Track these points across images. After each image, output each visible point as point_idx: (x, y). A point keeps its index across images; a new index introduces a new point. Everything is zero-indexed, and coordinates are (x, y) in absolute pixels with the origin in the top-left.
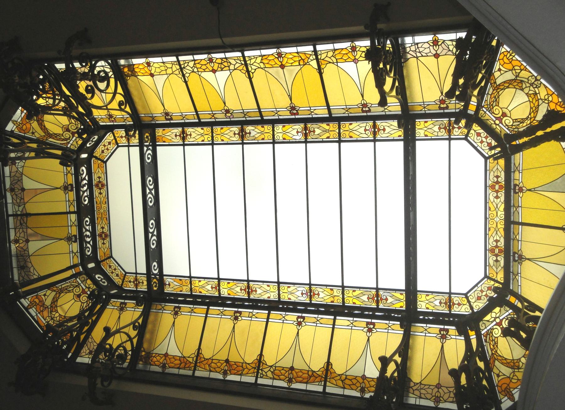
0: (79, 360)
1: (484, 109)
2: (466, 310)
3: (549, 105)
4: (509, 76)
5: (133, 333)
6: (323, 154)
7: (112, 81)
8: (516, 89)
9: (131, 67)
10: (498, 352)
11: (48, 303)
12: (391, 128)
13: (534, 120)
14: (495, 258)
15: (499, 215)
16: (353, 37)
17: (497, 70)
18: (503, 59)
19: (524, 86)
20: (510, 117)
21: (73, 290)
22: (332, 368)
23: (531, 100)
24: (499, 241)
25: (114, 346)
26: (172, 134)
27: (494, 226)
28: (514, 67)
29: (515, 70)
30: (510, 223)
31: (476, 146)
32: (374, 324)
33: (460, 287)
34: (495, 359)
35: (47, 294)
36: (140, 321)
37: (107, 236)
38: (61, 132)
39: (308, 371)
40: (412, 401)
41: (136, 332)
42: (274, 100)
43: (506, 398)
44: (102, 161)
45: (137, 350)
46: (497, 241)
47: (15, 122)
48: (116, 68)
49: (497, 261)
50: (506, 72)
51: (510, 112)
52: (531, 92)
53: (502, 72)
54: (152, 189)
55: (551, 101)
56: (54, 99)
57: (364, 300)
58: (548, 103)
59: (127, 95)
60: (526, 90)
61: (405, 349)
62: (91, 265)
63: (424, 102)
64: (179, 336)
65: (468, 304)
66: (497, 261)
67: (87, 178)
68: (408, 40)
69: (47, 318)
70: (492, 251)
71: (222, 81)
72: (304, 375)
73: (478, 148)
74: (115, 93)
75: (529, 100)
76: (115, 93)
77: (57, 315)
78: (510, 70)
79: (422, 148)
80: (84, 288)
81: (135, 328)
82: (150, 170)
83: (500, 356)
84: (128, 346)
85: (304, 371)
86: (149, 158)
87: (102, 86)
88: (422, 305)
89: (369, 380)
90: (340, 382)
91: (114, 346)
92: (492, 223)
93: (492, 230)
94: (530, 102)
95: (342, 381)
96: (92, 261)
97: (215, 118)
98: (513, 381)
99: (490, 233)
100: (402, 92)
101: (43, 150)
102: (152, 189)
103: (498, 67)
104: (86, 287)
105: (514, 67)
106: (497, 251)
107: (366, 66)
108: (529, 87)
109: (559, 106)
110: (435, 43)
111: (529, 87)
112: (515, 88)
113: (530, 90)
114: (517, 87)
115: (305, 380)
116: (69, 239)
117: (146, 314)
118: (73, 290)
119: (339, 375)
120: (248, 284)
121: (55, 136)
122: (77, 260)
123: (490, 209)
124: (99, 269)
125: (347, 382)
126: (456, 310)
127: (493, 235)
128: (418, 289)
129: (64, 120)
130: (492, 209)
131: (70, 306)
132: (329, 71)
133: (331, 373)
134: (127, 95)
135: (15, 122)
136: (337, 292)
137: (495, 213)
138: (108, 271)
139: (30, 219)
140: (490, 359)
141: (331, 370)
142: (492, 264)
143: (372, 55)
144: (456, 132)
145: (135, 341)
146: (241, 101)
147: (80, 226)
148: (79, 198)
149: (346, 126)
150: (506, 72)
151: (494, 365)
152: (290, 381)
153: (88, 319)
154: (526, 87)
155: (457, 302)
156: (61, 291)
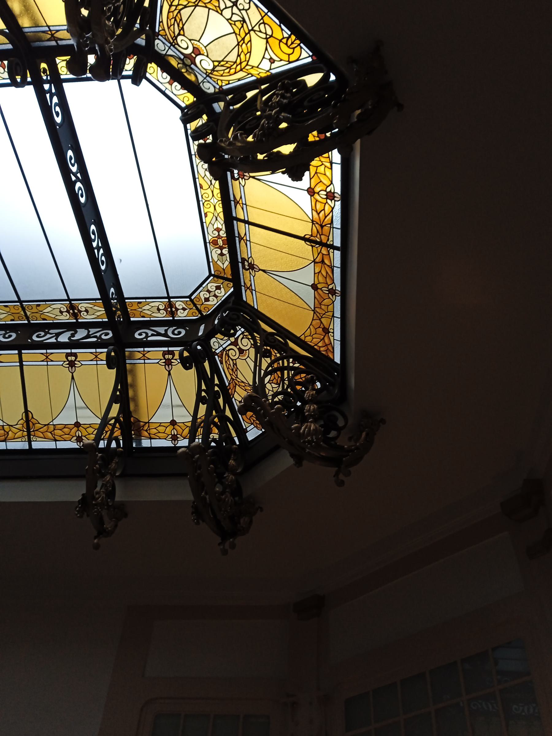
3: (267, 42)
8: (209, 9)
10: (240, 376)
13: (247, 65)
15: (212, 207)
22: (32, 417)
23: (237, 31)
24: (221, 230)
32: (75, 355)
34: (236, 384)
39: (3, 426)
40: (146, 443)
43: (252, 426)
49: (222, 254)
51: (205, 47)
52: (235, 18)
55: (271, 36)
58: (266, 39)
60: (227, 13)
61: (123, 394)
65: (194, 308)
66: (222, 254)
70: (215, 243)
75: (234, 32)
83: (242, 382)
89: (85, 426)
90: (49, 434)
92: (209, 206)
95: (51, 433)
98: (269, 32)
106: (220, 242)
108: (232, 7)
109: (286, 44)
111: (232, 7)
112: (206, 7)
119: (45, 425)
123: (201, 187)
126: (181, 315)
128: (125, 296)
130: (205, 186)
133: (34, 424)
137: (209, 191)
140: (229, 384)
142: (216, 259)
151: (235, 391)
154: (226, 8)
155: (181, 307)
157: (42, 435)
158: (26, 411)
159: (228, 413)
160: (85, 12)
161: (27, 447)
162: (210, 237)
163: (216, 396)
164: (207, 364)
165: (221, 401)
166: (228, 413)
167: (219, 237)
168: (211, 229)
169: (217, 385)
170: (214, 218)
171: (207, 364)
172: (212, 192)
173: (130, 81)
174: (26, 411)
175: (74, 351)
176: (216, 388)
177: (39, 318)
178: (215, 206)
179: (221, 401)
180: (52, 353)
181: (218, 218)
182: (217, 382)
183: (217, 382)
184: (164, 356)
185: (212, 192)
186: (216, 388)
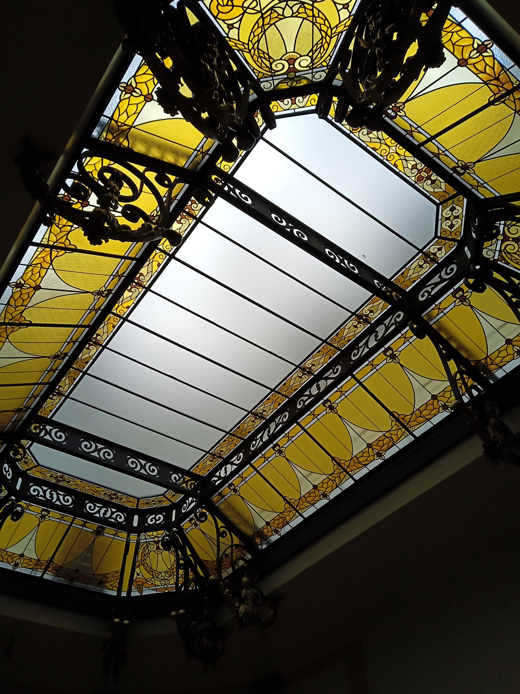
1: (261, 80)
2: (451, 246)
4: (250, 20)
8: (274, 24)
14: (429, 182)
17: (227, 30)
18: (219, 12)
19: (280, 11)
20: (301, 56)
21: (149, 550)
23: (305, 16)
24: (416, 164)
27: (397, 157)
28: (242, 7)
29: (248, 8)
31: (293, 111)
35: (139, 572)
36: (220, 524)
39: (384, 435)
44: (35, 467)
46: (414, 167)
49: (433, 182)
50: (241, 20)
52: (295, 9)
53: (236, 25)
54: (96, 447)
60: (288, 12)
63: (195, 150)
66: (433, 182)
67: (45, 488)
69: (161, 582)
70: (420, 179)
72: (385, 441)
73: (297, 111)
75: (304, 19)
77: (163, 574)
78: (243, 14)
80: (153, 540)
82: (74, 441)
85: (380, 439)
86: (61, 437)
93: (399, 163)
94: (306, 19)
96: (134, 518)
97: (57, 369)
99: (400, 167)
102: (96, 447)
103: (225, 27)
104: (154, 538)
105: (242, 7)
106: (424, 174)
108: (287, 4)
111: (287, 4)
112: (271, 25)
113: (291, 8)
114: (272, 22)
115: (391, 443)
116: (99, 532)
118: (149, 550)
120: (194, 217)
124: (143, 514)
125: (425, 413)
127: (405, 166)
130: (377, 146)
137: (384, 147)
141: (400, 417)
147: (90, 517)
148: (63, 509)
150: (241, 20)
152: (379, 455)
154: (284, 9)
155: (436, 250)
156: (143, 562)
162: (413, 178)
178: (397, 153)
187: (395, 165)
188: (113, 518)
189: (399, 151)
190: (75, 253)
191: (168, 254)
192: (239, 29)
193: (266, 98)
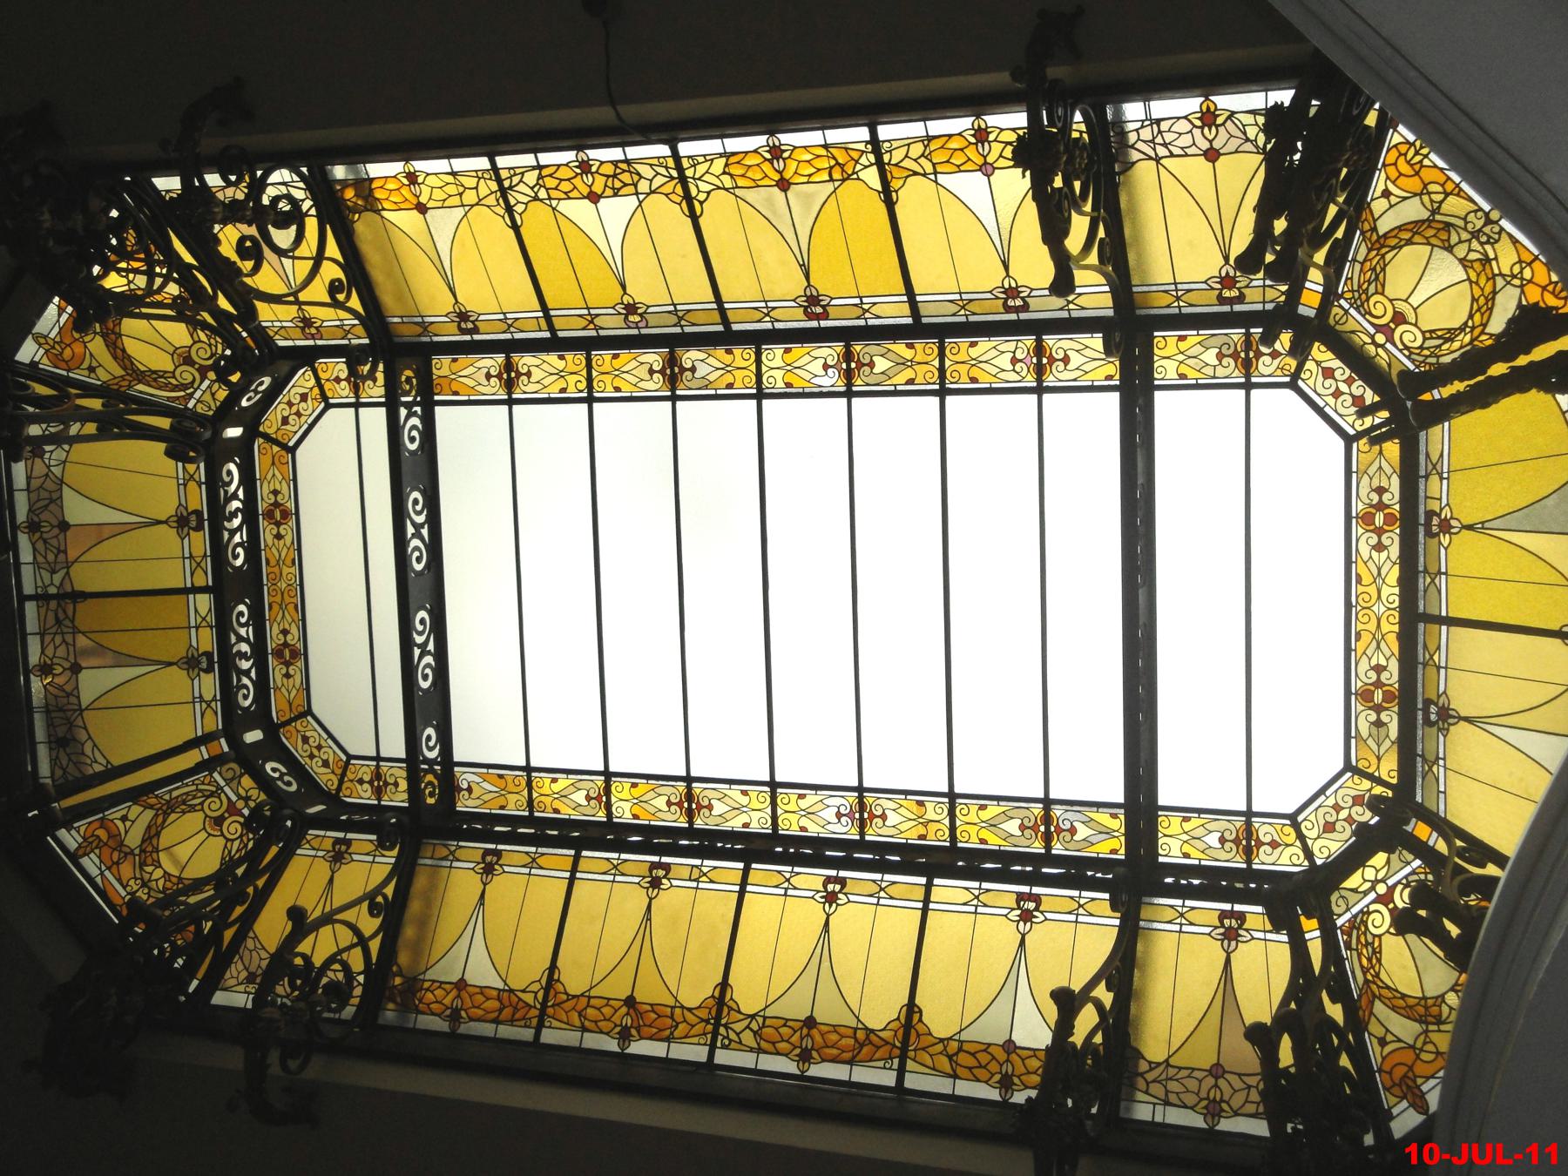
0: (219, 998)
2: (1294, 859)
3: (1523, 292)
4: (1414, 210)
5: (369, 925)
6: (896, 426)
7: (312, 224)
8: (1433, 246)
9: (364, 186)
10: (1383, 976)
11: (134, 839)
12: (1086, 355)
13: (1482, 333)
14: (1373, 717)
16: (978, 103)
17: (1378, 193)
18: (1395, 164)
19: (1454, 239)
20: (1415, 325)
21: (202, 804)
22: (920, 1020)
23: (1473, 277)
24: (1385, 668)
25: (318, 961)
26: (479, 370)
27: (1372, 626)
28: (1425, 186)
29: (1429, 193)
30: (1415, 618)
31: (1321, 404)
32: (1037, 899)
33: (1275, 796)
34: (1374, 996)
35: (132, 816)
36: (389, 891)
37: (297, 654)
38: (171, 368)
39: (856, 1029)
40: (1143, 1112)
41: (377, 922)
42: (761, 278)
45: (379, 972)
46: (1379, 669)
47: (41, 339)
48: (322, 189)
49: (1379, 724)
50: (1405, 198)
52: (1473, 256)
53: (1393, 200)
54: (422, 525)
56: (151, 275)
57: (1010, 834)
58: (1522, 286)
59: (354, 262)
60: (1461, 251)
62: (253, 736)
64: (497, 931)
66: (1379, 724)
67: (241, 493)
68: (1133, 111)
69: (132, 882)
70: (1366, 696)
71: (618, 224)
72: (844, 1041)
73: (1327, 410)
74: (319, 258)
75: (1468, 278)
76: (319, 258)
78: (1415, 195)
79: (1171, 412)
81: (373, 910)
82: (415, 472)
84: (356, 960)
85: (842, 1030)
86: (412, 440)
87: (283, 238)
88: (1172, 847)
90: (945, 1060)
91: (318, 961)
92: (1366, 619)
94: (1471, 282)
97: (597, 328)
99: (1361, 646)
100: (1116, 255)
101: (119, 415)
102: (422, 525)
103: (1381, 187)
105: (1425, 186)
107: (1015, 183)
108: (1469, 241)
110: (1208, 118)
111: (1469, 241)
112: (1428, 244)
113: (1470, 250)
114: (1433, 241)
116: (192, 663)
117: (404, 872)
118: (202, 804)
119: (942, 1040)
121: (153, 377)
122: (214, 722)
123: (1359, 580)
124: (274, 746)
125: (964, 1059)
129: (178, 333)
130: (1367, 579)
131: (195, 849)
132: (913, 196)
133: (918, 1035)
134: (354, 262)
135: (41, 339)
136: (936, 811)
137: (1372, 590)
138: (300, 752)
139: (83, 607)
140: (1360, 996)
141: (920, 1027)
142: (1365, 733)
143: (1032, 153)
144: (1266, 367)
145: (374, 946)
146: (668, 280)
147: (223, 626)
149: (960, 348)
150: (1405, 198)
151: (1371, 1013)
153: (244, 885)
154: (1460, 242)
156: (169, 808)
157: (929, 1062)
158: (553, 966)
159: (228, 934)
160: (114, 213)
161: (703, 1058)
162: (1360, 684)
163: (240, 897)
164: (274, 850)
165: (239, 910)
166: (228, 934)
167: (1378, 684)
168: (1364, 666)
169: (256, 888)
170: (1374, 644)
171: (274, 850)
172: (1379, 592)
173: (1096, 342)
174: (553, 966)
175: (665, 859)
176: (250, 890)
177: (510, 780)
178: (1379, 620)
179: (239, 910)
180: (1193, 908)
181: (1383, 644)
182: (260, 883)
183: (260, 883)
184: (825, 886)
185: (1379, 592)
186: (250, 890)
187: (1358, 635)
188: (239, 680)
189: (1384, 623)
190: (882, 208)
191: (529, 777)
192: (1391, 206)
193: (1316, 331)
